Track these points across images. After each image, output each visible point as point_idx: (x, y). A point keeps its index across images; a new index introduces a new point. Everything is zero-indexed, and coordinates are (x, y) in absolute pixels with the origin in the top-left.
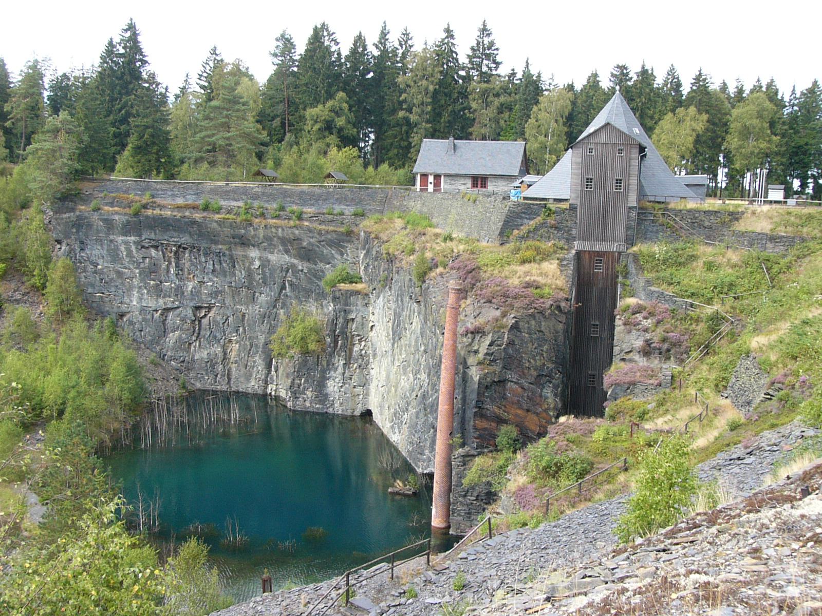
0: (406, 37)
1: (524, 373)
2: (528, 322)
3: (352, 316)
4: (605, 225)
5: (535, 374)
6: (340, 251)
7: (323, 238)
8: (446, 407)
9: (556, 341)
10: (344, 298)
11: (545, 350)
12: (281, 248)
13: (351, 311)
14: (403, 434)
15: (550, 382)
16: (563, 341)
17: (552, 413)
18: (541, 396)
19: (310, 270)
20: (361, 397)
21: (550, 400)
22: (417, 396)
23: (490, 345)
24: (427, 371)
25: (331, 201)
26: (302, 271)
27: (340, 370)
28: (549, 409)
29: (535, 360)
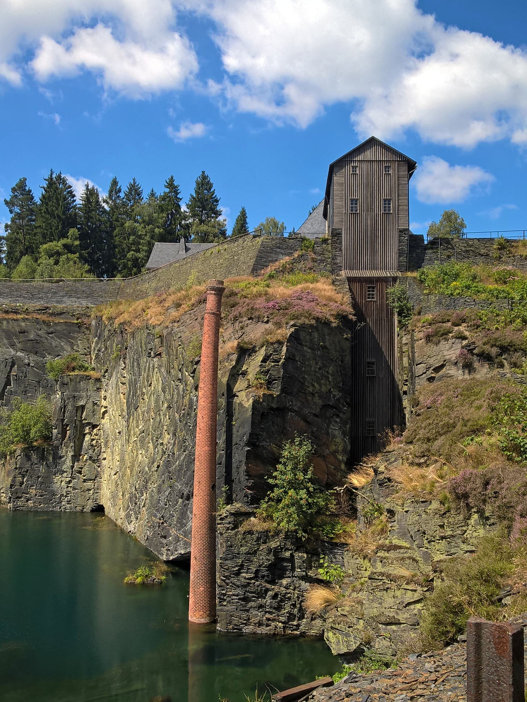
1: (307, 401)
2: (310, 334)
4: (374, 251)
5: (320, 402)
6: (69, 342)
7: (51, 330)
8: (207, 448)
9: (342, 362)
11: (331, 372)
12: (5, 341)
13: (80, 398)
14: (141, 519)
15: (338, 416)
16: (350, 363)
17: (340, 458)
18: (328, 434)
19: (37, 363)
20: (91, 492)
21: (338, 440)
22: (158, 467)
23: (264, 361)
25: (61, 294)
26: (29, 365)
27: (69, 463)
28: (336, 451)
29: (320, 385)
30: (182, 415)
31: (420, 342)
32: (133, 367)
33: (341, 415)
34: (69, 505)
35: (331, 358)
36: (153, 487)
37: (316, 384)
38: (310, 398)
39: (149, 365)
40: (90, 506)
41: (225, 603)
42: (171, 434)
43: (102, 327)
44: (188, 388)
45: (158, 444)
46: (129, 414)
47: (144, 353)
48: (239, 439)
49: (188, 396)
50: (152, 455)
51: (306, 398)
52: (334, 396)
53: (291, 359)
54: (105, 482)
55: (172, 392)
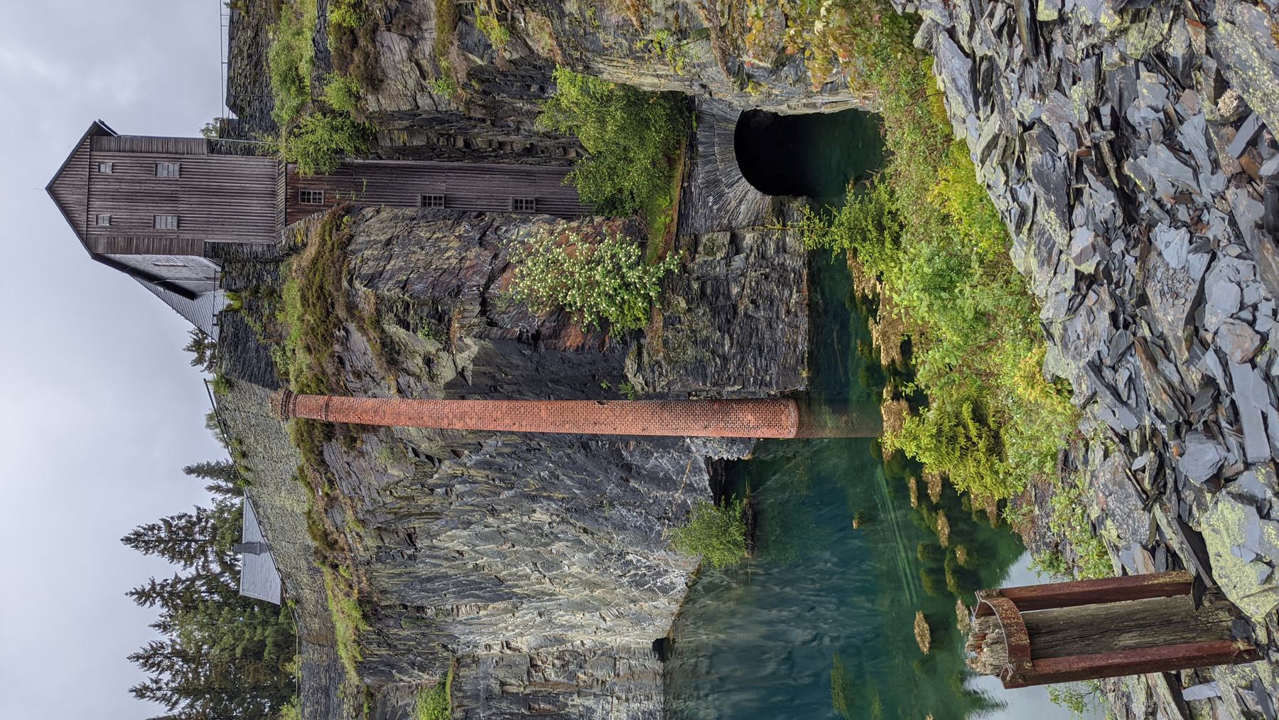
0: (148, 659)
1: (472, 267)
3: (496, 688)
4: (243, 193)
10: (465, 702)
11: (428, 235)
15: (498, 228)
22: (585, 531)
24: (525, 503)
27: (590, 702)
29: (447, 250)
30: (502, 484)
31: (383, 101)
32: (434, 591)
33: (496, 224)
34: (654, 698)
35: (406, 234)
36: (618, 541)
37: (447, 255)
38: (468, 263)
39: (428, 556)
40: (654, 664)
41: (768, 378)
42: (535, 506)
43: (374, 662)
44: (459, 472)
45: (552, 533)
46: (510, 596)
47: (410, 569)
48: (529, 364)
49: (472, 472)
50: (569, 544)
51: (467, 268)
52: (467, 231)
53: (405, 285)
54: (618, 640)
55: (468, 508)
